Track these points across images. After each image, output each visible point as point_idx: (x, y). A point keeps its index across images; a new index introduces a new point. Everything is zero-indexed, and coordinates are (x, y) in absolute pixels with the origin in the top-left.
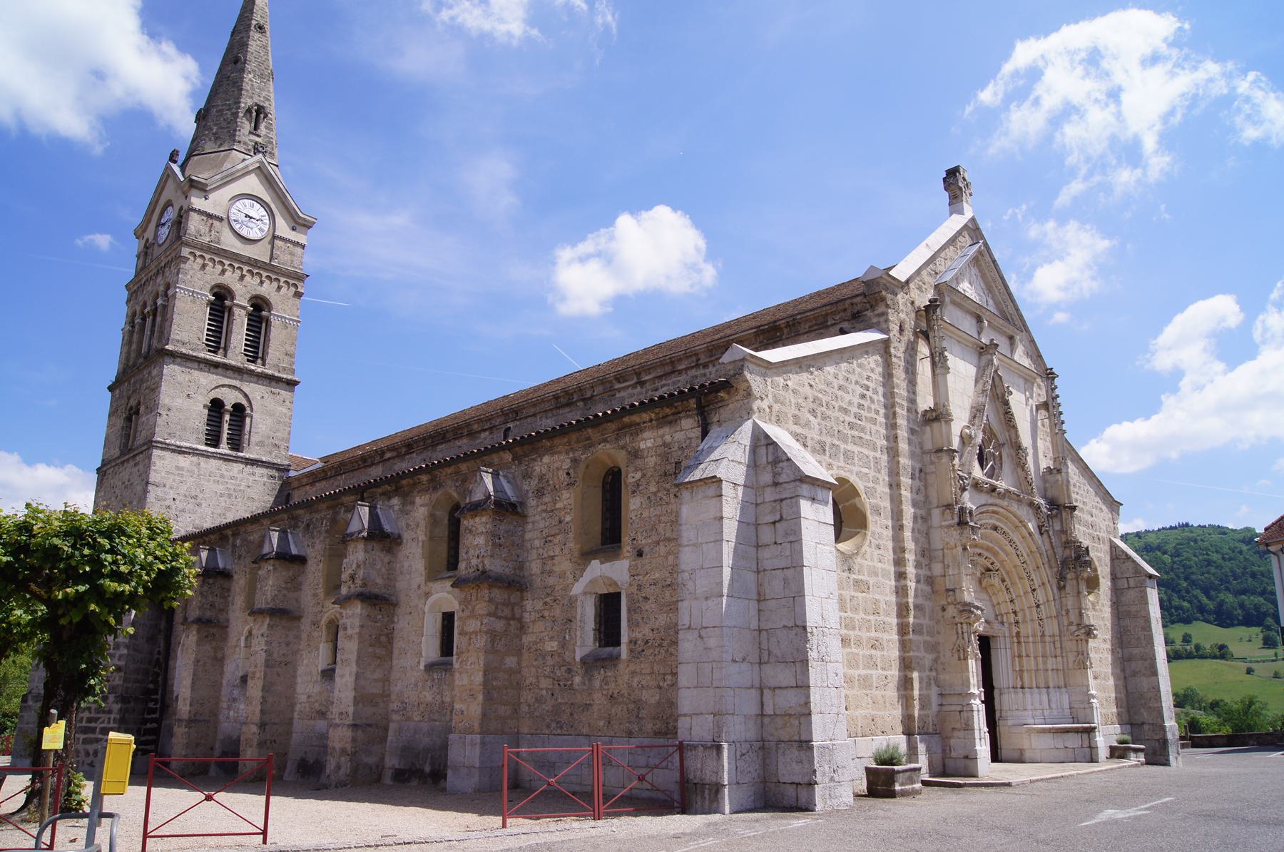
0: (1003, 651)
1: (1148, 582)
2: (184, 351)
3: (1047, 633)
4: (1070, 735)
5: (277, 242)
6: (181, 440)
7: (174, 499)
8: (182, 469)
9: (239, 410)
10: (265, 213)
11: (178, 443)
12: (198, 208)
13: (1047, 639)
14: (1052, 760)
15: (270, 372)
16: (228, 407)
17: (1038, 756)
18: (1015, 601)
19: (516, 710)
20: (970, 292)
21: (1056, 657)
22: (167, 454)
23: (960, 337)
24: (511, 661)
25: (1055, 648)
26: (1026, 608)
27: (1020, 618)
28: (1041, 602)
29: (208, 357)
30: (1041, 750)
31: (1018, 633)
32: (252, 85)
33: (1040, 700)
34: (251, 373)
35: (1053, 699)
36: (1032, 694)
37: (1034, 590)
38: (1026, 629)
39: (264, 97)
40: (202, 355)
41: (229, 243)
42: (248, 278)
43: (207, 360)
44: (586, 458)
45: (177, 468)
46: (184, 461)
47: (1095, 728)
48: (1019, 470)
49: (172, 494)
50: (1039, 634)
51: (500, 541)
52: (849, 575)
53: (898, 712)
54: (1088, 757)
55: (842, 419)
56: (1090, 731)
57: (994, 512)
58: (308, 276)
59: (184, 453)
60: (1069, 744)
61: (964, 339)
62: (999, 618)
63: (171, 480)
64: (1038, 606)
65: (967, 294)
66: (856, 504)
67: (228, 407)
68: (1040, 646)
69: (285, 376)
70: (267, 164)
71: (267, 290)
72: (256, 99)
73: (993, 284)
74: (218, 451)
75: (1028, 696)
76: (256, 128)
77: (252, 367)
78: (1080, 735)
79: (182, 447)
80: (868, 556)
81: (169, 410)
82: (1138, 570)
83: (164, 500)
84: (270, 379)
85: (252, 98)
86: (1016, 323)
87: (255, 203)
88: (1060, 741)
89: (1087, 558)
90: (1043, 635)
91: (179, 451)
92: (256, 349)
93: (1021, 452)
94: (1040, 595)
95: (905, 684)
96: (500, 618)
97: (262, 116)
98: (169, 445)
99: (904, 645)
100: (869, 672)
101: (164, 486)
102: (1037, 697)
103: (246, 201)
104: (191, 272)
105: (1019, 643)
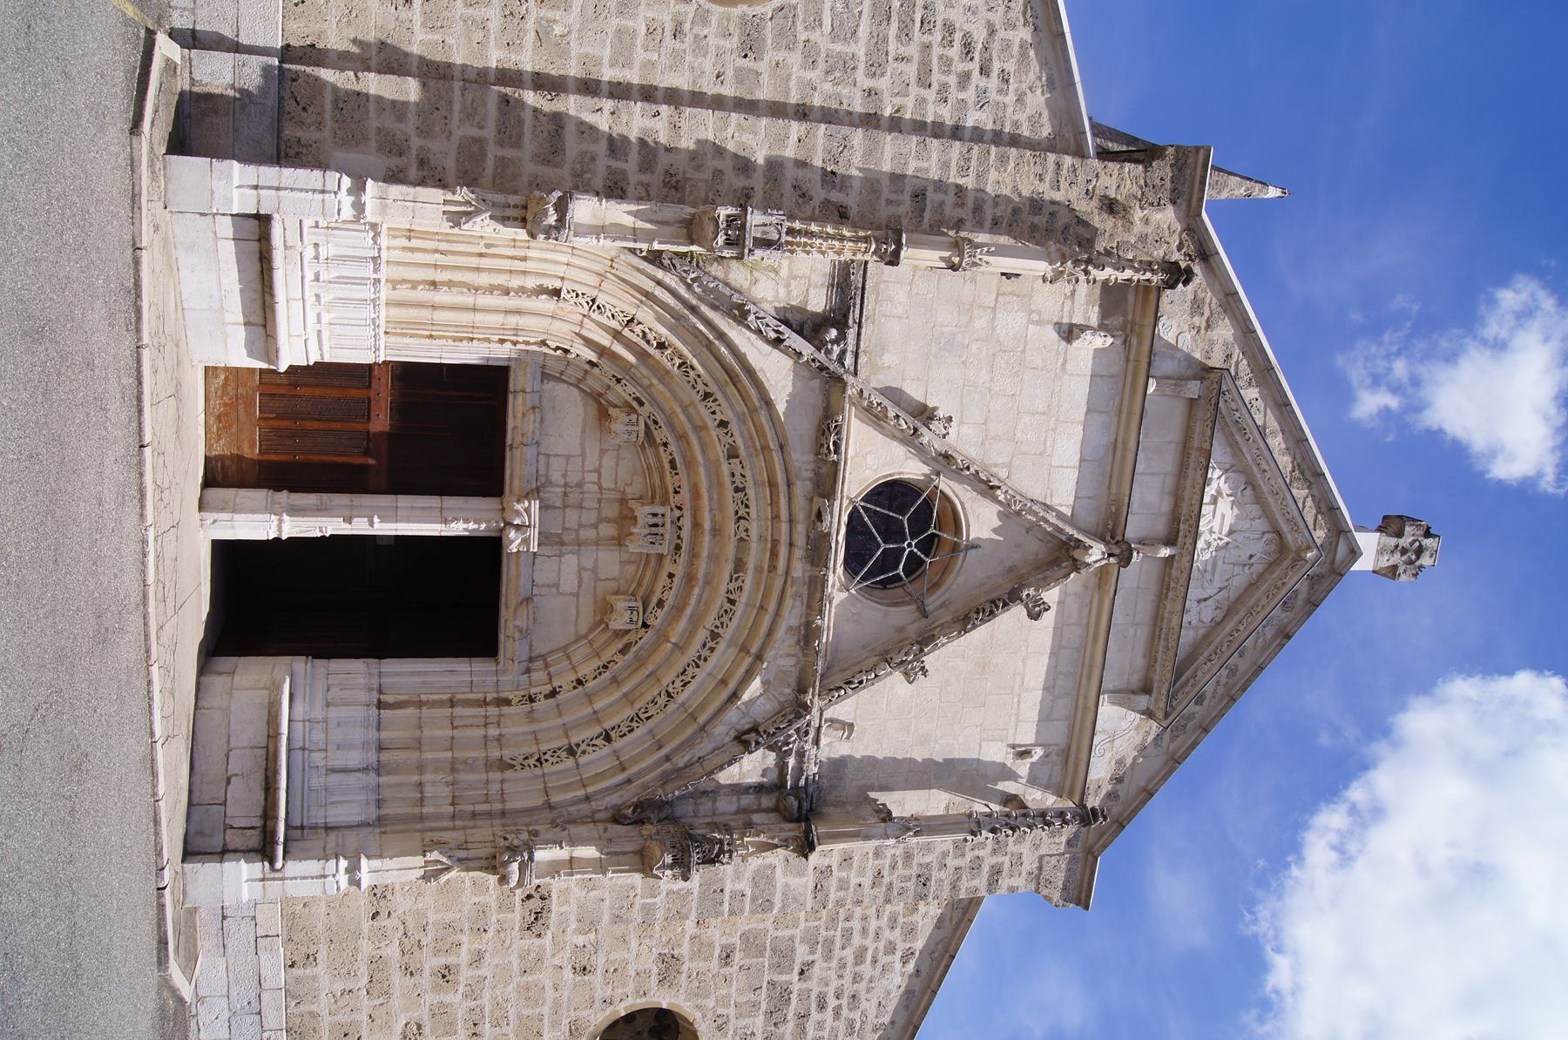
3: (508, 774)
4: (260, 795)
14: (201, 738)
17: (213, 700)
20: (1216, 525)
23: (1125, 443)
26: (559, 721)
27: (542, 705)
28: (582, 760)
30: (227, 711)
35: (352, 779)
36: (365, 745)
37: (608, 738)
38: (515, 724)
44: (773, 838)
47: (272, 862)
53: (335, 39)
54: (199, 843)
56: (264, 851)
60: (236, 790)
61: (1124, 457)
64: (571, 752)
65: (1206, 510)
68: (479, 754)
73: (1242, 613)
75: (359, 713)
78: (258, 823)
86: (1180, 696)
88: (244, 762)
89: (695, 857)
90: (504, 765)
94: (597, 759)
95: (389, 59)
99: (481, 78)
102: (358, 735)
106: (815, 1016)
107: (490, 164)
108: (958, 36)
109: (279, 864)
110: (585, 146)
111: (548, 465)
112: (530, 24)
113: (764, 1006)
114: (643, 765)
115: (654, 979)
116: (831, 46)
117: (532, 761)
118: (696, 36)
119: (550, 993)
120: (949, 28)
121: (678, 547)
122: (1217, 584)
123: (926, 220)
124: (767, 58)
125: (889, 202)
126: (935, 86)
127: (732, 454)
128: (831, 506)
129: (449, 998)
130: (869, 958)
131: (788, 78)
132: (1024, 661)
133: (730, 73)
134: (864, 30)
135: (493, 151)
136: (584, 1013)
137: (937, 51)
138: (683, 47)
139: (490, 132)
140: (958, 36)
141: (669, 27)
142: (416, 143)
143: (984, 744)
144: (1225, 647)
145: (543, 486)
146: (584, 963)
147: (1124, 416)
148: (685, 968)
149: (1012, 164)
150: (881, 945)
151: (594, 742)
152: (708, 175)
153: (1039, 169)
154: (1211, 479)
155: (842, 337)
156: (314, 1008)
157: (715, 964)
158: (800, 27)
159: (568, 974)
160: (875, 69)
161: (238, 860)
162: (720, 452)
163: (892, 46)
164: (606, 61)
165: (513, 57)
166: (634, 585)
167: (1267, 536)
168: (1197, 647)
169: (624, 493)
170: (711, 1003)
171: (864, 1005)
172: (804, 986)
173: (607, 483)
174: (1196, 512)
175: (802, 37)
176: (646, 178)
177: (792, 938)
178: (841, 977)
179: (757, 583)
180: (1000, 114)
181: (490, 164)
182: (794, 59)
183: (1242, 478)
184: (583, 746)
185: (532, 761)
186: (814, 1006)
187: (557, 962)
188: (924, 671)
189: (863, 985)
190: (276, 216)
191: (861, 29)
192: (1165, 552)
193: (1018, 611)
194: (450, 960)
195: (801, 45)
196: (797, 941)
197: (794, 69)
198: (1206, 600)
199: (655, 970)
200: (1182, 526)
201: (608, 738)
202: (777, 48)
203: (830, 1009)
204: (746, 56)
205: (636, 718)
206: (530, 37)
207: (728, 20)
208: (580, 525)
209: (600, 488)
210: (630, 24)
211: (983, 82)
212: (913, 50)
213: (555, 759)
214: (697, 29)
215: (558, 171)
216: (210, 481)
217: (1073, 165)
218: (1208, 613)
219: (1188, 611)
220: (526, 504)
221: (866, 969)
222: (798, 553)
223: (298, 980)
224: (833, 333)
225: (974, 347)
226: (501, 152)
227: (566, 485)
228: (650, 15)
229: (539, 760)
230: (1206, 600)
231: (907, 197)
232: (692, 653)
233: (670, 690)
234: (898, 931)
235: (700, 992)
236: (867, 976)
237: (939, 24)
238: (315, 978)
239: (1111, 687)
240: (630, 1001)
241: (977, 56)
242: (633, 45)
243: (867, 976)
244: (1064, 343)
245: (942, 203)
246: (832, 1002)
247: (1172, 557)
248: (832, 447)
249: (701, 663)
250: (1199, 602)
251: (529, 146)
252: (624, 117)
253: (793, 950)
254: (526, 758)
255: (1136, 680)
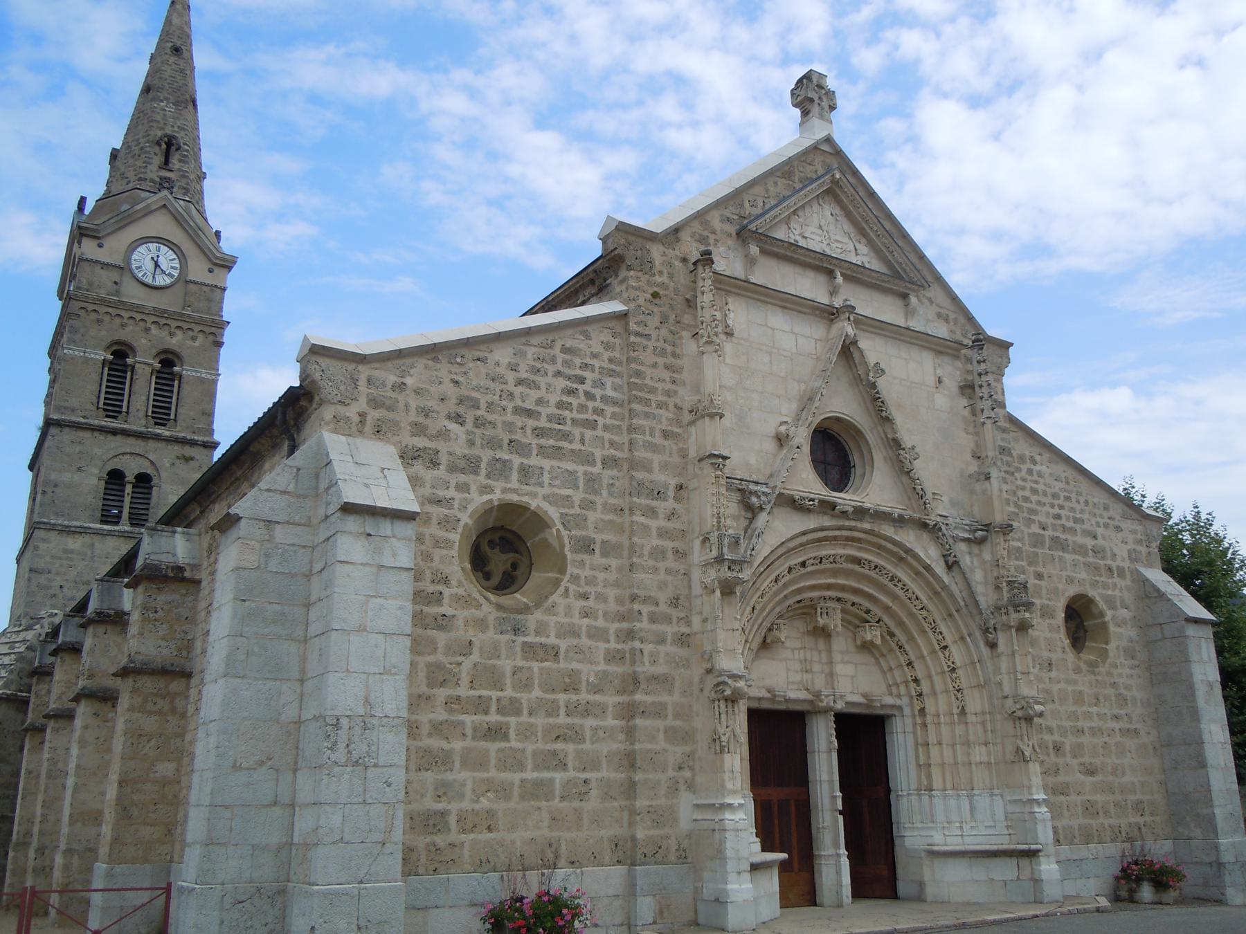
0: (901, 737)
1: (1191, 631)
2: (73, 419)
3: (967, 710)
5: (192, 287)
6: (70, 519)
7: (61, 587)
8: (71, 551)
9: (143, 480)
10: (175, 256)
11: (66, 523)
12: (89, 257)
13: (971, 718)
15: (181, 435)
16: (130, 478)
18: (915, 665)
19: (169, 831)
20: (818, 238)
21: (986, 744)
22: (53, 536)
24: (165, 769)
25: (985, 731)
28: (958, 664)
29: (103, 423)
31: (922, 711)
32: (164, 115)
33: (959, 808)
34: (158, 438)
37: (945, 647)
39: (179, 127)
40: (96, 422)
41: (133, 294)
42: (155, 330)
43: (102, 427)
45: (66, 551)
46: (74, 543)
48: (905, 479)
49: (59, 581)
50: (956, 711)
51: (157, 616)
52: (514, 638)
55: (519, 424)
57: (853, 539)
58: (228, 323)
59: (74, 532)
62: (894, 689)
63: (57, 565)
64: (953, 670)
66: (547, 540)
67: (130, 478)
69: (201, 438)
70: (172, 199)
71: (176, 341)
72: (169, 131)
73: (865, 226)
74: (117, 528)
76: (167, 162)
77: (159, 430)
78: (1014, 861)
79: (71, 527)
80: (561, 610)
81: (56, 486)
82: (1176, 612)
83: (50, 588)
84: (182, 442)
85: (163, 129)
87: (162, 246)
90: (963, 712)
91: (67, 531)
92: (161, 414)
93: (902, 452)
96: (151, 713)
97: (173, 148)
98: (55, 525)
100: (546, 775)
101: (49, 572)
102: (952, 802)
103: (150, 245)
104: (82, 330)
105: (925, 725)
106: (1063, 521)
107: (678, 723)
108: (565, 398)
109: (1039, 847)
110: (662, 660)
111: (793, 683)
112: (592, 698)
113: (1061, 554)
114: (962, 627)
115: (1052, 621)
116: (581, 489)
117: (959, 695)
118: (586, 584)
119: (1062, 685)
120: (560, 405)
121: (839, 600)
122: (846, 240)
123: (678, 430)
124: (593, 535)
125: (671, 455)
126: (595, 417)
127: (803, 564)
128: (840, 504)
129: (1068, 748)
130: (1035, 486)
131: (602, 520)
132: (895, 378)
133: (604, 561)
134: (570, 466)
135: (670, 722)
136: (1070, 665)
137: (575, 415)
138: (593, 593)
139: (660, 724)
140: (565, 398)
141: (582, 603)
142: (671, 773)
143: (936, 407)
144: (886, 241)
145: (803, 686)
146: (1047, 664)
147: (769, 300)
148: (1046, 602)
149: (640, 368)
150: (1029, 478)
151: (947, 656)
152: (670, 578)
153: (641, 348)
154: (795, 240)
155: (755, 493)
156: (1076, 827)
157: (1043, 583)
158: (571, 512)
159: (1053, 674)
160: (590, 460)
161: (1040, 871)
162: (803, 571)
163: (576, 446)
164: (607, 646)
165: (611, 709)
166: (850, 627)
167: (821, 202)
168: (887, 263)
169: (804, 633)
170: (1060, 586)
171: (1057, 490)
172: (1050, 528)
173: (798, 645)
174: (819, 255)
175: (577, 510)
176: (675, 620)
177: (1029, 534)
178: (1044, 504)
179: (866, 550)
180: (605, 371)
181: (678, 723)
182: (592, 516)
183: (793, 217)
184: (950, 663)
185: (959, 695)
186: (1058, 522)
187: (1047, 681)
188: (913, 448)
189: (1048, 490)
190: (751, 860)
191: (569, 468)
192: (840, 279)
193: (882, 383)
194: (1051, 746)
195: (583, 511)
196: (1030, 531)
197: (597, 516)
198: (856, 250)
199: (1047, 621)
200: (825, 265)
201: (945, 647)
202: (586, 528)
203: (1060, 512)
204: (593, 550)
205: (934, 630)
206: (598, 698)
207: (575, 561)
208: (820, 662)
209: (801, 648)
210: (584, 629)
211: (589, 382)
212: (576, 431)
213: (958, 681)
214: (583, 583)
215: (677, 678)
216: (815, 904)
217: (635, 323)
218: (863, 249)
219: (863, 263)
220: (823, 697)
221: (1040, 487)
222: (859, 525)
223: (1065, 838)
224: (754, 499)
225: (740, 401)
226: (670, 716)
227: (802, 671)
228: (577, 615)
229: (958, 691)
230: (856, 250)
231: (666, 443)
232: (901, 593)
233: (920, 608)
234: (1021, 466)
235: (1055, 591)
236: (1043, 488)
237: (560, 412)
238: (1064, 828)
239: (903, 320)
240: (1062, 636)
241: (575, 386)
242: (595, 627)
243: (1043, 488)
244: (733, 339)
245: (668, 419)
246: (1056, 511)
247: (842, 274)
248: (811, 503)
249: (906, 588)
250: (857, 254)
251: (665, 698)
252: (643, 634)
253: (1034, 534)
254: (957, 699)
255: (899, 302)
